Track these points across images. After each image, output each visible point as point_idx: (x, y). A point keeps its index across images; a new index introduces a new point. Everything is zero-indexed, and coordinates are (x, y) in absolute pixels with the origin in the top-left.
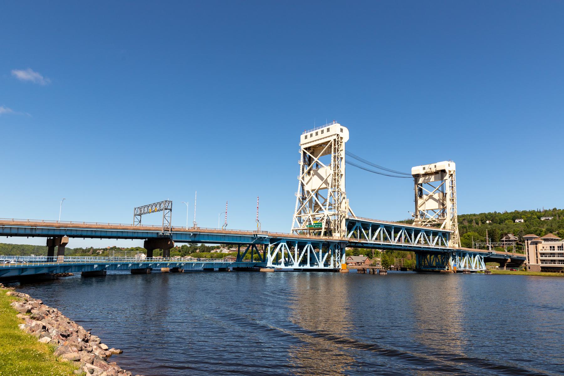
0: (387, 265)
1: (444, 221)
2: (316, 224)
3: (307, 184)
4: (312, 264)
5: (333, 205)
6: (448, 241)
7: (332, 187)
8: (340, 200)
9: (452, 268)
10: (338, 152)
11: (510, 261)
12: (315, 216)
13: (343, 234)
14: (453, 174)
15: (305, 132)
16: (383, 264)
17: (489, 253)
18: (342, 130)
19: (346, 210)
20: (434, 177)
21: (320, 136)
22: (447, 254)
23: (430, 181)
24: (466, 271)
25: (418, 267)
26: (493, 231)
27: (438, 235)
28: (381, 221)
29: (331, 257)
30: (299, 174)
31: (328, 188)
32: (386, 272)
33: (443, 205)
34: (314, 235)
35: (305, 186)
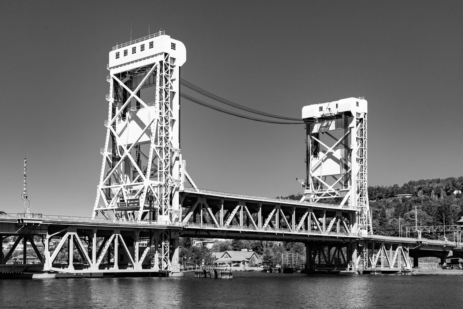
1: (346, 194)
2: (130, 200)
3: (119, 135)
4: (121, 266)
6: (351, 225)
7: (156, 141)
11: (452, 255)
12: (132, 188)
14: (364, 119)
16: (264, 262)
17: (418, 242)
18: (173, 46)
20: (335, 123)
21: (139, 54)
22: (350, 246)
23: (330, 130)
24: (374, 271)
25: (308, 267)
26: (446, 208)
27: (336, 216)
29: (155, 253)
30: (107, 118)
33: (346, 167)
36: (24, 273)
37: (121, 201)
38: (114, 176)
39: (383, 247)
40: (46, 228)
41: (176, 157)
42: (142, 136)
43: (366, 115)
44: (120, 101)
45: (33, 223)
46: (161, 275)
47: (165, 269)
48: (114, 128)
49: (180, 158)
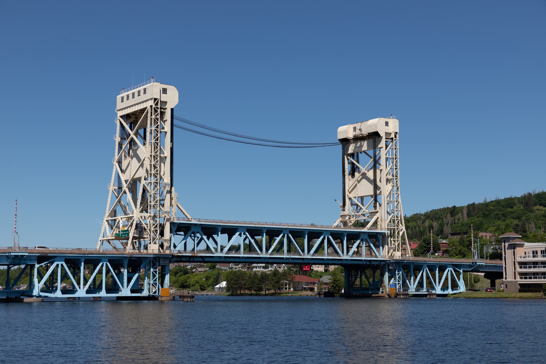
0: (337, 288)
6: (381, 248)
9: (388, 290)
18: (165, 91)
27: (361, 238)
29: (145, 279)
38: (122, 208)
39: (425, 269)
42: (137, 173)
43: (398, 134)
45: (19, 255)
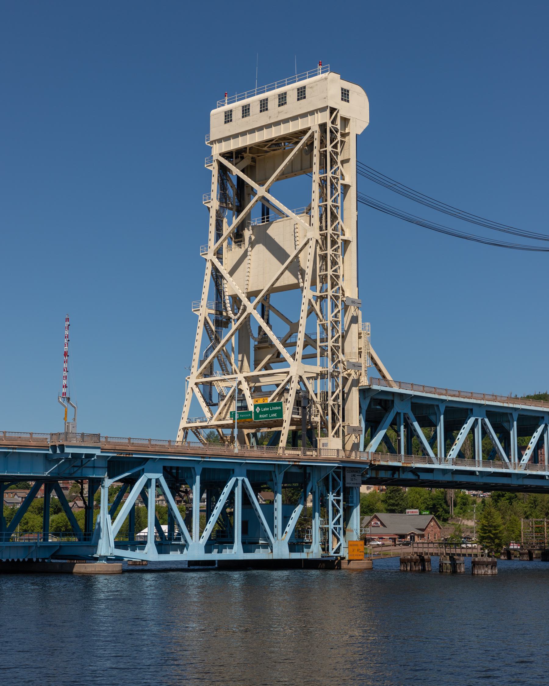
2: (261, 406)
3: (232, 273)
5: (319, 343)
7: (313, 284)
8: (340, 325)
10: (335, 168)
13: (352, 439)
15: (227, 97)
18: (345, 95)
19: (362, 361)
28: (449, 392)
31: (301, 285)
32: (494, 565)
34: (255, 444)
35: (225, 282)
36: (53, 561)
37: (239, 408)
40: (104, 464)
41: (353, 317)
44: (230, 205)
46: (324, 565)
47: (335, 553)
48: (220, 259)
49: (360, 319)
